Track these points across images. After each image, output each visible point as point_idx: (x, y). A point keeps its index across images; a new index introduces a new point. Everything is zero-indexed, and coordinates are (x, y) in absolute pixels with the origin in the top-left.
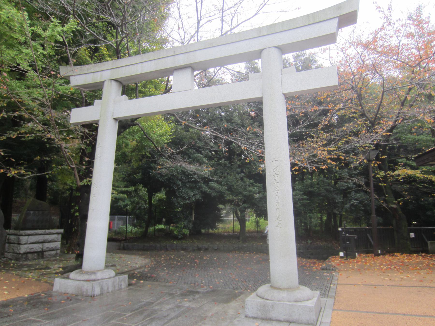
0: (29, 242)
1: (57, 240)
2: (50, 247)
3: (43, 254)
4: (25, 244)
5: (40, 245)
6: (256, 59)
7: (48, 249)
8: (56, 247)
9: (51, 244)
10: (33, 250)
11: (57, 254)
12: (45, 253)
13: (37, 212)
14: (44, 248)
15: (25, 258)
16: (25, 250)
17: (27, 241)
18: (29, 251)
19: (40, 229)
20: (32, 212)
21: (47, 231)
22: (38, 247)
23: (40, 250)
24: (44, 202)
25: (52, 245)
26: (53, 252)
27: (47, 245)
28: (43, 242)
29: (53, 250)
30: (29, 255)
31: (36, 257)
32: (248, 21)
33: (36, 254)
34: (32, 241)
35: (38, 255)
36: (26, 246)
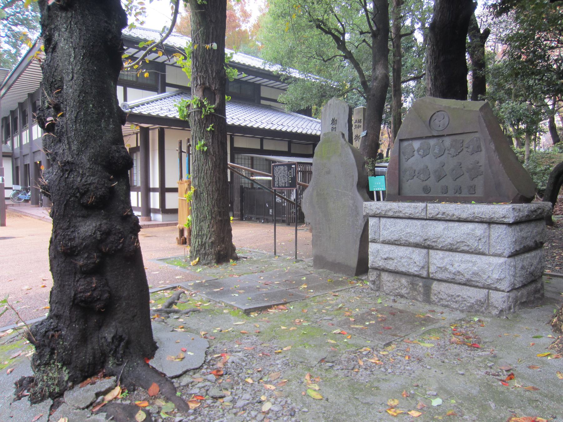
5: (418, 255)
8: (475, 274)
9: (458, 257)
10: (391, 265)
11: (485, 304)
12: (435, 286)
13: (432, 142)
20: (416, 144)
21: (435, 208)
23: (414, 270)
25: (461, 264)
26: (473, 295)
27: (438, 259)
28: (426, 246)
29: (467, 283)
30: (385, 277)
31: (404, 291)
33: (404, 281)
35: (413, 285)
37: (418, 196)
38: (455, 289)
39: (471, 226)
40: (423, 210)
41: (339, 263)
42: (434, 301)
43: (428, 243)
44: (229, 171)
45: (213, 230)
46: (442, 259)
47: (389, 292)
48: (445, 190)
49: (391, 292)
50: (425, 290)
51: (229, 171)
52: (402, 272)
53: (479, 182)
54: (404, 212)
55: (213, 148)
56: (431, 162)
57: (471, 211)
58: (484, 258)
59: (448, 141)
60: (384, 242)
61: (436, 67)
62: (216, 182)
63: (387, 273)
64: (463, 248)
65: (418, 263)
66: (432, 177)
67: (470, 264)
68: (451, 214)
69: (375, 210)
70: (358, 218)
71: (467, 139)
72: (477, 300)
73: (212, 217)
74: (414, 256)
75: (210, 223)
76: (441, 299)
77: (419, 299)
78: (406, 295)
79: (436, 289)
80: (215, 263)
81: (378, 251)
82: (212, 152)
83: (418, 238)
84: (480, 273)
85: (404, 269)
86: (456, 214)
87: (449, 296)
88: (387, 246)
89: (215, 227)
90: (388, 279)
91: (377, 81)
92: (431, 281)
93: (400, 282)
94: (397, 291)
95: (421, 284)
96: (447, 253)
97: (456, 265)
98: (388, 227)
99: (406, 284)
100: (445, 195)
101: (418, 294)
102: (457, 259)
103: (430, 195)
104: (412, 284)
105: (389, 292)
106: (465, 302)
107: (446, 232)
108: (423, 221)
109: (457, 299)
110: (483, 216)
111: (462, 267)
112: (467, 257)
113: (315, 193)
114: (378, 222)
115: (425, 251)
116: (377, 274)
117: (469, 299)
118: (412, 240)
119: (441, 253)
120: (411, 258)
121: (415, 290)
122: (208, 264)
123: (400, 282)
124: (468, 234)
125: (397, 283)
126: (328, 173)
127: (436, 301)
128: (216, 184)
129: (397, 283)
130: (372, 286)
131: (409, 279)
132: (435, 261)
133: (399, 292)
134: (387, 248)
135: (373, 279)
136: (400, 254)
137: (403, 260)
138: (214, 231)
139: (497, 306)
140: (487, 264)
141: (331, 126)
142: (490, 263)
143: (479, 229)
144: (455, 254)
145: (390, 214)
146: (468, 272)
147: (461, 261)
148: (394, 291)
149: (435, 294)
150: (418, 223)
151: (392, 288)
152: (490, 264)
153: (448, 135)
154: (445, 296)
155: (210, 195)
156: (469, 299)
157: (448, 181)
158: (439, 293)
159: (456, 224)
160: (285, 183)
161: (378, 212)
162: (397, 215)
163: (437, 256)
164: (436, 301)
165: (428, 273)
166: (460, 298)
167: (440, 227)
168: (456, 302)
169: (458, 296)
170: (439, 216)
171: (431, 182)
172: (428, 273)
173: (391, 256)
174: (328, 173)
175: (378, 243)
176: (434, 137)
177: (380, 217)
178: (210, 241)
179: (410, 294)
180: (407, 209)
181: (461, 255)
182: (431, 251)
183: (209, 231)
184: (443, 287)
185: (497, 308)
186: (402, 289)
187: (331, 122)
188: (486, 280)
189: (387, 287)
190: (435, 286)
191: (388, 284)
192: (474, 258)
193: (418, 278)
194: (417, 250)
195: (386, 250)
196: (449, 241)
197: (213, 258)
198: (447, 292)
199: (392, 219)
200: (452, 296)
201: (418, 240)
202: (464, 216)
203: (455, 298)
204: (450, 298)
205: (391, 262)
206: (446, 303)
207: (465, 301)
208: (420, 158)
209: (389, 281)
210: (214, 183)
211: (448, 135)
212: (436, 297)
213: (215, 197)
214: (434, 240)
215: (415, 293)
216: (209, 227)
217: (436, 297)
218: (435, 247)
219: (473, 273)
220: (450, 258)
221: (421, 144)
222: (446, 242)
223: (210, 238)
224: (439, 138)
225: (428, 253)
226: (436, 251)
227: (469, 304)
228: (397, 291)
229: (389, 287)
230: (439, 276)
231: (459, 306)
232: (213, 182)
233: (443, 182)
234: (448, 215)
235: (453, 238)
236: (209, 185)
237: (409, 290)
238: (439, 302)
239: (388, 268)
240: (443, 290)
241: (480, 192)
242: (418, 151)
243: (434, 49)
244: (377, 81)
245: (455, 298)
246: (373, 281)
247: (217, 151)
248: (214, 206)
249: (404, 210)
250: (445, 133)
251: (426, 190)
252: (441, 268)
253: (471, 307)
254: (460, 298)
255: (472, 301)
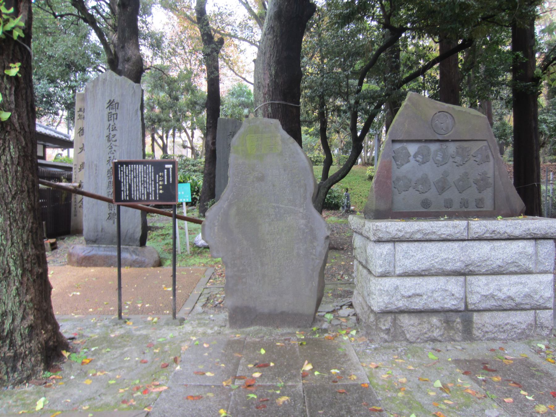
0: (398, 271)
1: (531, 266)
2: (501, 295)
3: (468, 326)
4: (384, 275)
5: (454, 285)
6: (365, 125)
7: (492, 303)
8: (527, 296)
9: (505, 280)
10: (418, 304)
11: (536, 325)
12: (476, 317)
13: (433, 147)
14: (473, 299)
15: (388, 331)
16: (386, 299)
17: (393, 263)
18: (401, 304)
19: (453, 216)
20: (413, 148)
21: (478, 226)
22: (444, 292)
23: (450, 304)
24: (456, 107)
25: (510, 287)
26: (521, 319)
27: (482, 287)
28: (464, 273)
29: (518, 308)
30: (405, 320)
31: (436, 334)
32: (123, 290)
33: (435, 320)
34: (409, 264)
35: (448, 323)
36: (388, 283)
37: (417, 212)
38: (501, 318)
39: (521, 243)
40: (465, 229)
41: (282, 313)
42: (478, 337)
43: (471, 269)
44: (166, 171)
45: (28, 297)
46: (487, 284)
47: (414, 339)
48: (449, 203)
49: (418, 338)
50: (464, 326)
51: (166, 171)
52: (433, 309)
53: (488, 195)
54: (439, 233)
55: (19, 116)
56: (432, 172)
57: (524, 228)
58: (532, 277)
59: (452, 148)
60: (400, 276)
61: (278, 62)
62: (28, 192)
63: (406, 316)
64: (511, 269)
65: (458, 295)
66: (433, 190)
67: (521, 286)
68: (502, 232)
69: (394, 232)
70: (315, 244)
71: (475, 147)
72: (529, 324)
73: (24, 270)
74: (449, 287)
75: (21, 283)
76: (487, 332)
77: (457, 339)
78: (440, 338)
79: (479, 321)
80: (45, 370)
81: (397, 288)
82: (17, 125)
83: (458, 264)
84: (532, 294)
85: (436, 306)
86: (508, 231)
87: (496, 327)
88: (408, 279)
89: (32, 290)
90: (412, 322)
91: (131, 63)
92: (470, 313)
93: (429, 323)
94: (426, 336)
95: (458, 320)
96: (490, 277)
97: (505, 289)
98: (411, 253)
99: (438, 324)
100: (450, 210)
101: (456, 333)
102: (504, 283)
103: (432, 209)
104: (447, 322)
105: (414, 339)
106: (515, 330)
107: (493, 254)
108: (461, 243)
109: (505, 328)
110: (538, 232)
111: (512, 291)
112: (514, 278)
113: (233, 211)
114: (392, 249)
115: (462, 278)
116: (392, 319)
117: (519, 325)
118: (449, 267)
119: (483, 280)
120: (446, 290)
121: (452, 328)
122: (28, 378)
123: (429, 323)
124: (521, 253)
125: (426, 326)
126: (261, 179)
127: (481, 336)
128: (29, 196)
129: (426, 326)
130: (386, 337)
131: (442, 317)
132: (478, 289)
133: (430, 337)
134: (409, 282)
135: (387, 327)
136: (431, 287)
137: (435, 295)
138: (31, 300)
139: (548, 326)
140: (537, 283)
141: (108, 111)
142: (540, 282)
143: (528, 246)
144: (499, 277)
145: (418, 236)
146: (519, 295)
147: (510, 284)
148: (422, 337)
149: (479, 328)
150: (456, 245)
151: (419, 333)
152: (540, 283)
153: (453, 141)
154: (491, 328)
155: (15, 220)
156: (519, 325)
157: (452, 194)
158: (484, 326)
159: (503, 243)
160: (148, 194)
161: (400, 234)
162: (427, 237)
163: (480, 283)
164: (481, 336)
165: (466, 305)
166: (509, 327)
167: (485, 248)
168: (504, 332)
169: (506, 324)
170: (487, 235)
171: (432, 194)
172: (466, 305)
173: (418, 292)
174: (261, 179)
175: (392, 276)
176: (438, 141)
177: (394, 242)
178: (26, 324)
179: (445, 336)
180: (443, 229)
181: (507, 277)
182: (469, 278)
183: (21, 303)
184: (486, 317)
185: (547, 328)
186: (433, 332)
187: (106, 106)
188: (537, 301)
189: (411, 334)
190: (476, 317)
191: (413, 329)
192: (524, 278)
193: (451, 313)
194: (453, 279)
195: (410, 285)
196: (498, 263)
197: (36, 360)
198: (493, 323)
199: (416, 244)
200: (500, 325)
201: (458, 266)
202: (517, 233)
203: (502, 328)
204: (496, 329)
205: (417, 300)
206: (493, 335)
207: (516, 328)
208: (416, 165)
209: (413, 325)
210: (25, 194)
211: (453, 141)
212: (480, 331)
213: (28, 225)
214: (479, 264)
215: (452, 333)
216: (18, 294)
217: (480, 331)
218: (477, 272)
219: (525, 296)
220: (496, 283)
221: (419, 148)
222: (494, 265)
223: (23, 318)
224: (442, 143)
225: (465, 280)
226: (475, 277)
227: (519, 331)
228: (426, 336)
229: (415, 332)
230: (483, 305)
231: (508, 336)
232: (22, 192)
233: (447, 195)
234: (499, 233)
235: (503, 260)
236: (13, 198)
237: (443, 330)
238: (484, 336)
239: (413, 307)
240: (488, 321)
241: (488, 206)
242: (415, 156)
243: (276, 41)
244: (131, 63)
245: (502, 328)
246: (387, 329)
247: (27, 123)
248: (25, 245)
249: (440, 230)
250: (450, 139)
251: (426, 203)
252: (486, 296)
253: (522, 333)
254: (509, 327)
255: (524, 326)
